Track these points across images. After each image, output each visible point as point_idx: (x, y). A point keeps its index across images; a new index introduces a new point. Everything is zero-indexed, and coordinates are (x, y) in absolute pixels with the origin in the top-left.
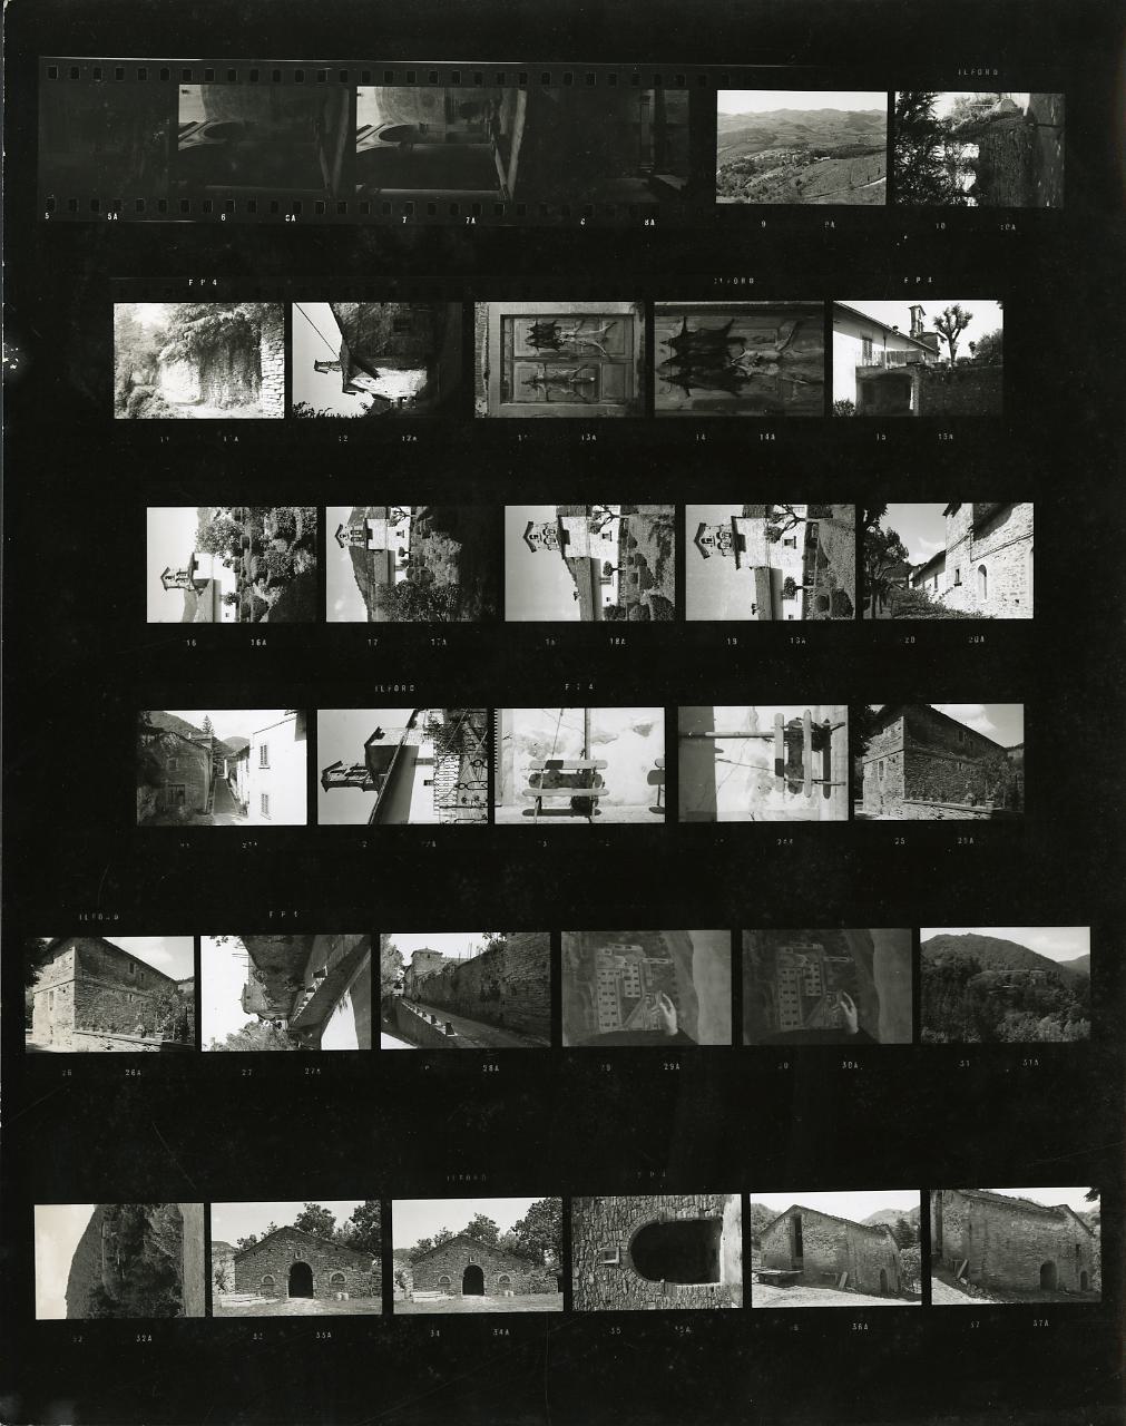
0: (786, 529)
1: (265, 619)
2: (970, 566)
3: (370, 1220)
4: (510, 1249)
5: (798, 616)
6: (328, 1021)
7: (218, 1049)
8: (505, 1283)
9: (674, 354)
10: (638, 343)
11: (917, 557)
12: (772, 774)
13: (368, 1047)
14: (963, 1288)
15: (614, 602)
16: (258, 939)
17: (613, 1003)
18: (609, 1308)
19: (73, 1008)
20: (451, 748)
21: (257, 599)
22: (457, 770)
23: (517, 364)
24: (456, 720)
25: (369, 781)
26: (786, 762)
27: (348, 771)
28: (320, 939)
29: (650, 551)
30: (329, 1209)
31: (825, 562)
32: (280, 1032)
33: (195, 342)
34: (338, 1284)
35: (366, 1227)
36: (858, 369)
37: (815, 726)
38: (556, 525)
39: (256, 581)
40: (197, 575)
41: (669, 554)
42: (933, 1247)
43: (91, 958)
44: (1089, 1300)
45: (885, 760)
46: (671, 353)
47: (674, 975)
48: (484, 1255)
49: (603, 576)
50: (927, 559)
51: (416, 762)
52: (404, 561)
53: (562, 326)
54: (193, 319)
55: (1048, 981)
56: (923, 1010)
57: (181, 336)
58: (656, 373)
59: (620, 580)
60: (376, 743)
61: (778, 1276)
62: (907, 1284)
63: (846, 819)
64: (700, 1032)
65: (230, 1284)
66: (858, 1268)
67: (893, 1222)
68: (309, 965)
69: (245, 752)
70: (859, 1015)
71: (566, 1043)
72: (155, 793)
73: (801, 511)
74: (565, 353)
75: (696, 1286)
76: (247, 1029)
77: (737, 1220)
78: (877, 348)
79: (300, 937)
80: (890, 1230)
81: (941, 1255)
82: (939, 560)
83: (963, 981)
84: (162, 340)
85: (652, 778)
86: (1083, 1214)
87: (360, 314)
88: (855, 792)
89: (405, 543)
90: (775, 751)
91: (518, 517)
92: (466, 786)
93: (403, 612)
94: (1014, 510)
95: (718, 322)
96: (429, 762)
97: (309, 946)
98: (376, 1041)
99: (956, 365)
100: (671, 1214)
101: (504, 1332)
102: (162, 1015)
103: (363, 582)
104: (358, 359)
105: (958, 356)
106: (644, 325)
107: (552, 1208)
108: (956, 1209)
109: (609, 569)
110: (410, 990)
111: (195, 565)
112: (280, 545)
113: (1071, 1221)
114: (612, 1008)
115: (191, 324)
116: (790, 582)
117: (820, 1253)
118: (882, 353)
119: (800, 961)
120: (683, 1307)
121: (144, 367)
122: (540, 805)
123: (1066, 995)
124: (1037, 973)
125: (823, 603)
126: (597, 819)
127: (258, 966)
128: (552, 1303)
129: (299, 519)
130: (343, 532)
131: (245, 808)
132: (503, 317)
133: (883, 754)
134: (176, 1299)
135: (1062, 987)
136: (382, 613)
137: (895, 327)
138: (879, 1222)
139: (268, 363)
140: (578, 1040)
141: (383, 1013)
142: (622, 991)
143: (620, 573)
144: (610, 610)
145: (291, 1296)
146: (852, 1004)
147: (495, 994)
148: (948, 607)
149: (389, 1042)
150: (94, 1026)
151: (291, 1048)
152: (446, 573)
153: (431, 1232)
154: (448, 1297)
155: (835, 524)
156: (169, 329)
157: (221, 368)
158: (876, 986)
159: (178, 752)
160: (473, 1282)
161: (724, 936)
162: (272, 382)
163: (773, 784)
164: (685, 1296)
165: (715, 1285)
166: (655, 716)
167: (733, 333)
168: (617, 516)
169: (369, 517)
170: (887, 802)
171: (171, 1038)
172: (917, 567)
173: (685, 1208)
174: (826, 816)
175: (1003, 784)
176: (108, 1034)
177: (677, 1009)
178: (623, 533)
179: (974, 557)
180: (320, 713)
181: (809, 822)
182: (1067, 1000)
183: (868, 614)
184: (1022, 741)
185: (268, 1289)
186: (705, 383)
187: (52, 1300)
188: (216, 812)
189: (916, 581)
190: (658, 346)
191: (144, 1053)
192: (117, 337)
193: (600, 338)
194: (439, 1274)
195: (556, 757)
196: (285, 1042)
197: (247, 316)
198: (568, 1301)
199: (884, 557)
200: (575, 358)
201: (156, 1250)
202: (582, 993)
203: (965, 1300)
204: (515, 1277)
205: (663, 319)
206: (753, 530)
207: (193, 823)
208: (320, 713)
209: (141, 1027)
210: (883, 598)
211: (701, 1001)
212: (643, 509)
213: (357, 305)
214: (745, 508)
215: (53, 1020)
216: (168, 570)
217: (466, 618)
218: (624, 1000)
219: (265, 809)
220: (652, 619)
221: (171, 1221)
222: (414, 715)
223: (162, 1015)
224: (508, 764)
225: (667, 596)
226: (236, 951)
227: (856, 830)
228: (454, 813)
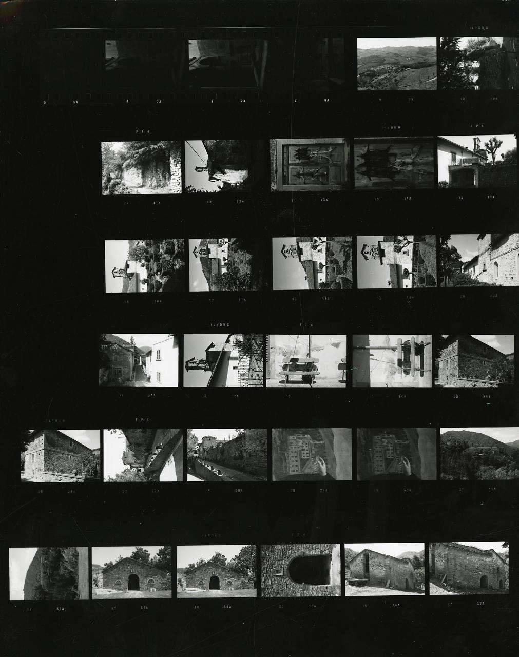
0: (404, 247)
1: (161, 290)
2: (490, 262)
3: (166, 555)
4: (232, 568)
5: (410, 286)
6: (163, 468)
7: (111, 481)
8: (229, 584)
9: (364, 161)
10: (346, 156)
11: (465, 259)
12: (396, 366)
13: (182, 480)
14: (444, 588)
15: (324, 280)
16: (130, 431)
17: (296, 461)
18: (278, 596)
19: (44, 462)
20: (246, 352)
21: (157, 281)
22: (249, 362)
23: (290, 167)
24: (249, 340)
25: (208, 367)
26: (403, 360)
27: (198, 362)
28: (159, 431)
29: (341, 258)
30: (147, 550)
31: (422, 261)
32: (140, 473)
33: (140, 158)
34: (151, 584)
35: (164, 558)
36: (449, 167)
37: (416, 344)
38: (297, 246)
39: (157, 273)
40: (129, 271)
41: (349, 258)
42: (430, 568)
43: (52, 439)
44: (503, 593)
45: (449, 360)
46: (362, 161)
47: (325, 449)
48: (219, 571)
49: (318, 269)
50: (470, 259)
51: (229, 358)
52: (225, 263)
53: (311, 149)
54: (139, 148)
55: (500, 452)
56: (442, 465)
57: (132, 156)
58: (355, 170)
59: (326, 271)
60: (211, 349)
61: (357, 582)
62: (418, 586)
63: (431, 386)
64: (337, 475)
65: (100, 584)
66: (395, 578)
67: (411, 557)
68: (224, 468)
69: (150, 353)
70: (411, 467)
71: (274, 479)
72: (108, 371)
73: (411, 238)
74: (312, 162)
75: (319, 586)
76: (124, 472)
77: (338, 556)
78: (458, 157)
79: (150, 430)
80: (410, 561)
81: (434, 573)
82: (475, 260)
83: (460, 452)
84: (123, 158)
85: (340, 367)
86: (501, 554)
87: (216, 145)
88: (435, 374)
89: (226, 255)
90: (398, 355)
91: (278, 243)
92: (253, 370)
93: (225, 287)
94: (510, 237)
95: (384, 147)
96: (235, 358)
97: (154, 434)
98: (185, 477)
99: (495, 164)
100: (308, 553)
101: (229, 607)
102: (85, 465)
103: (206, 273)
104: (215, 166)
105: (496, 160)
106: (349, 148)
107: (252, 550)
108: (442, 554)
109: (321, 266)
110: (201, 455)
111: (127, 266)
112: (167, 257)
113: (495, 557)
114: (296, 464)
115: (137, 151)
116: (406, 270)
117: (377, 571)
118: (461, 159)
119: (384, 442)
120: (313, 596)
121: (116, 171)
122: (288, 379)
123: (509, 458)
124: (495, 448)
125: (422, 280)
126: (314, 386)
127: (130, 443)
128: (251, 593)
129: (176, 244)
130: (197, 250)
131: (149, 378)
132: (283, 146)
133: (448, 357)
134: (75, 591)
135: (506, 455)
136: (216, 287)
137: (467, 148)
138: (405, 557)
139: (174, 168)
140: (280, 478)
141: (189, 465)
142: (300, 456)
143: (327, 267)
144: (322, 284)
145: (129, 590)
146: (409, 462)
147: (241, 457)
148: (480, 281)
149: (191, 478)
150: (53, 470)
151: (145, 481)
152: (245, 268)
153: (195, 561)
154: (202, 590)
155: (427, 244)
156: (127, 153)
157: (152, 171)
158: (420, 455)
159: (118, 353)
160: (215, 584)
161: (348, 431)
162: (175, 177)
163: (397, 370)
164: (314, 590)
165: (328, 585)
166: (342, 339)
167: (391, 151)
168: (325, 242)
169: (209, 243)
170: (450, 378)
171: (89, 476)
172: (465, 263)
173: (314, 550)
174: (421, 385)
175: (504, 371)
176: (60, 474)
177: (326, 464)
178: (328, 249)
179: (492, 258)
180: (185, 336)
181: (413, 388)
182: (509, 461)
183: (443, 285)
184: (513, 352)
185: (118, 586)
186: (377, 174)
187: (17, 591)
188: (136, 380)
189: (465, 269)
190: (356, 158)
191: (77, 482)
192: (103, 157)
193: (328, 155)
194: (199, 580)
195: (295, 357)
196: (143, 478)
197: (164, 147)
198: (259, 592)
199: (450, 259)
200: (317, 164)
201: (66, 568)
202: (282, 457)
203: (445, 593)
204: (234, 581)
205: (358, 145)
206: (388, 247)
207: (125, 385)
208: (185, 336)
209: (75, 471)
210: (450, 278)
211: (337, 460)
212: (337, 239)
213: (215, 141)
214: (384, 238)
215: (34, 467)
216: (115, 269)
217: (255, 289)
218: (302, 460)
219: (159, 379)
220: (342, 288)
221: (73, 555)
222: (229, 337)
223: (85, 465)
224: (273, 360)
225: (348, 278)
226: (120, 436)
227: (436, 391)
228: (247, 382)
